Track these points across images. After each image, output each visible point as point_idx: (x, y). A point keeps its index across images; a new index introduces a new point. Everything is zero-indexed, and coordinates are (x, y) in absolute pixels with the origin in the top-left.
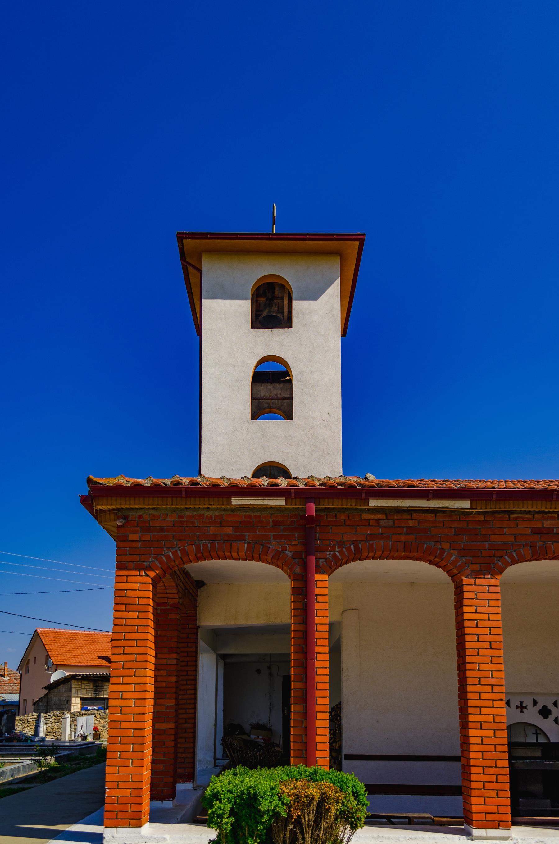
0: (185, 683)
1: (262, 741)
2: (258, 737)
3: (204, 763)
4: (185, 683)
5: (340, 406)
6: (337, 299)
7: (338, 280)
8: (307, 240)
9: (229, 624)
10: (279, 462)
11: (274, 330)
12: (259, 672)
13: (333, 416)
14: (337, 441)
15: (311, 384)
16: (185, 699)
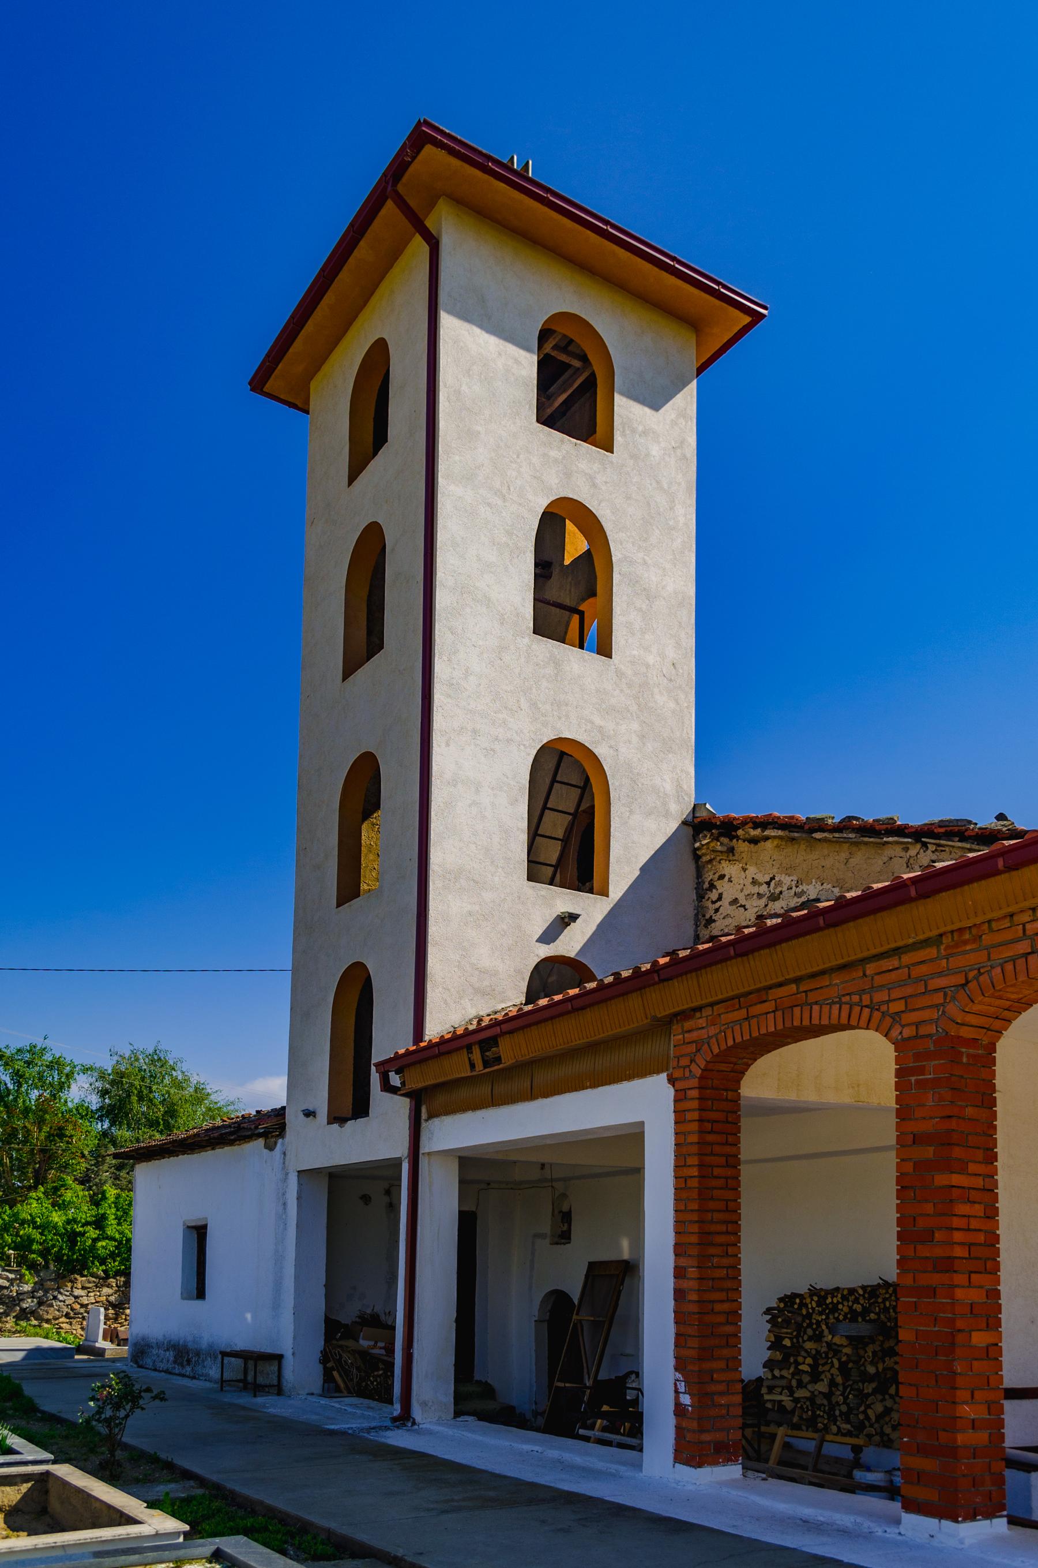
0: (723, 1228)
1: (383, 1352)
2: (376, 1343)
3: (433, 1408)
4: (723, 1228)
5: (692, 655)
6: (689, 423)
7: (692, 383)
8: (667, 272)
9: (787, 1098)
10: (586, 744)
11: (580, 445)
12: (366, 1199)
13: (681, 671)
14: (687, 728)
15: (645, 589)
16: (724, 1267)
